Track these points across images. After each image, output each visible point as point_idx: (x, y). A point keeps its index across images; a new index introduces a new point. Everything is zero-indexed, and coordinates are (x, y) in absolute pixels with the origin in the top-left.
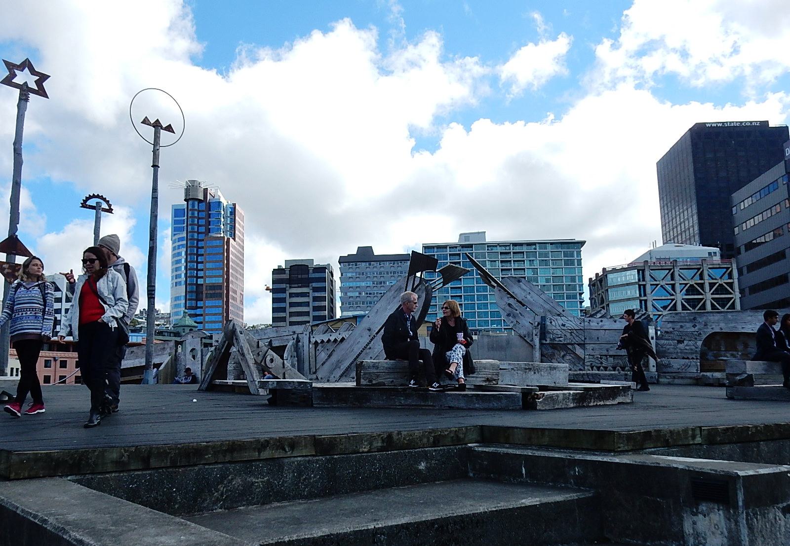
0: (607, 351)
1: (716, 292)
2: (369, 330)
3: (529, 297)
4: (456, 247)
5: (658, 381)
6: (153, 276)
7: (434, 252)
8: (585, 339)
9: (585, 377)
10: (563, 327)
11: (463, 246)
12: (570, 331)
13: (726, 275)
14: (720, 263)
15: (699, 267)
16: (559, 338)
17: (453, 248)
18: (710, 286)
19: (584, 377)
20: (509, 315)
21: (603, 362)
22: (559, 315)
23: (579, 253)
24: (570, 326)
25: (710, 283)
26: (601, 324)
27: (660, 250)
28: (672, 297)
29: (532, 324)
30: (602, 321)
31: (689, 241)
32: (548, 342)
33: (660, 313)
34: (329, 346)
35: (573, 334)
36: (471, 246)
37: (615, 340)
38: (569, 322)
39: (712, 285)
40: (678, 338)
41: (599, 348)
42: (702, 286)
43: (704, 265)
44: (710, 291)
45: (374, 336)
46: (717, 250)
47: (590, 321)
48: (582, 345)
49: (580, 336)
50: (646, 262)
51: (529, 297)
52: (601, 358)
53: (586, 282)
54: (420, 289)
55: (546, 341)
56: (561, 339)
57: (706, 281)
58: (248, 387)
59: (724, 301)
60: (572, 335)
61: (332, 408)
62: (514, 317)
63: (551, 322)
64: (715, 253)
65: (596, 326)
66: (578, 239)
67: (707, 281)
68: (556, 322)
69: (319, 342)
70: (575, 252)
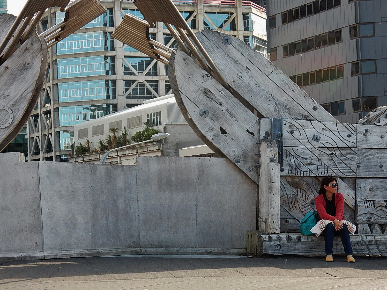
3: (246, 77)
6: (111, 44)
8: (359, 167)
12: (328, 152)
13: (228, 24)
15: (191, 9)
16: (309, 164)
19: (371, 247)
20: (204, 114)
22: (306, 118)
24: (329, 140)
29: (252, 134)
35: (334, 158)
38: (327, 133)
41: (383, 187)
43: (199, 7)
47: (367, 131)
49: (348, 162)
51: (246, 77)
54: (27, 49)
60: (331, 159)
62: (216, 118)
63: (292, 132)
68: (302, 131)
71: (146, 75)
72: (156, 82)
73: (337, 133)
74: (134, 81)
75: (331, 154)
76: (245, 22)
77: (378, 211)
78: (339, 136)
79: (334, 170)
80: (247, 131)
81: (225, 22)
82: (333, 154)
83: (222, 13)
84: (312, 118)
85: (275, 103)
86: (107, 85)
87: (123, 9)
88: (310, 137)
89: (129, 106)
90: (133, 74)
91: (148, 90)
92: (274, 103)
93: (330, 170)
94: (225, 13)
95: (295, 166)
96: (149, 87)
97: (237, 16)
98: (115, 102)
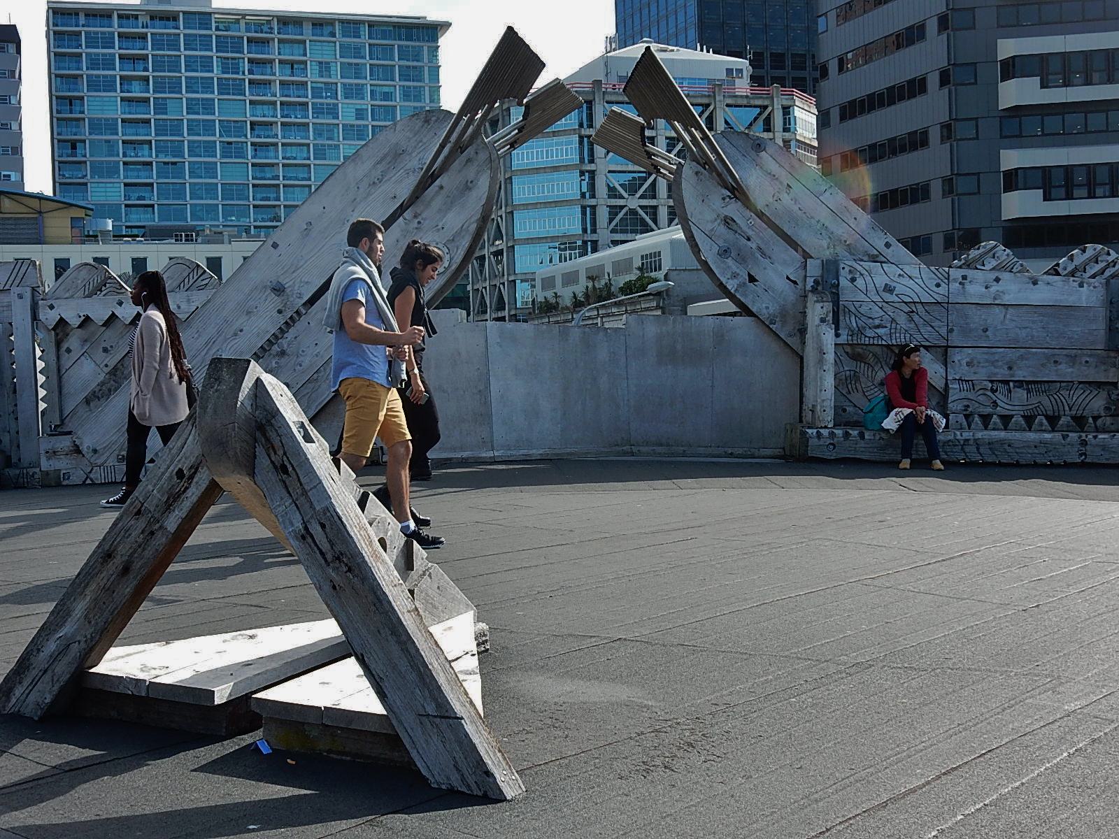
0: (1010, 368)
2: (279, 290)
3: (786, 198)
4: (136, 17)
7: (77, 25)
9: (971, 449)
11: (154, 16)
13: (760, 122)
14: (749, 94)
15: (705, 101)
16: (878, 327)
17: (128, 17)
26: (995, 288)
27: (625, 56)
31: (675, 40)
33: (621, 202)
34: (110, 336)
35: (916, 318)
36: (170, 18)
37: (1033, 337)
38: (906, 281)
41: (987, 361)
45: (298, 312)
46: (742, 63)
47: (964, 277)
48: (944, 353)
50: (597, 83)
52: (993, 391)
56: (881, 331)
58: (394, 741)
62: (742, 259)
63: (853, 280)
64: (740, 71)
65: (982, 296)
66: (433, 16)
69: (75, 322)
70: (425, 49)
72: (655, 208)
74: (622, 207)
76: (785, 119)
78: (923, 286)
80: (788, 278)
82: (913, 312)
83: (750, 106)
86: (584, 213)
89: (616, 243)
91: (643, 220)
97: (773, 110)
98: (594, 237)
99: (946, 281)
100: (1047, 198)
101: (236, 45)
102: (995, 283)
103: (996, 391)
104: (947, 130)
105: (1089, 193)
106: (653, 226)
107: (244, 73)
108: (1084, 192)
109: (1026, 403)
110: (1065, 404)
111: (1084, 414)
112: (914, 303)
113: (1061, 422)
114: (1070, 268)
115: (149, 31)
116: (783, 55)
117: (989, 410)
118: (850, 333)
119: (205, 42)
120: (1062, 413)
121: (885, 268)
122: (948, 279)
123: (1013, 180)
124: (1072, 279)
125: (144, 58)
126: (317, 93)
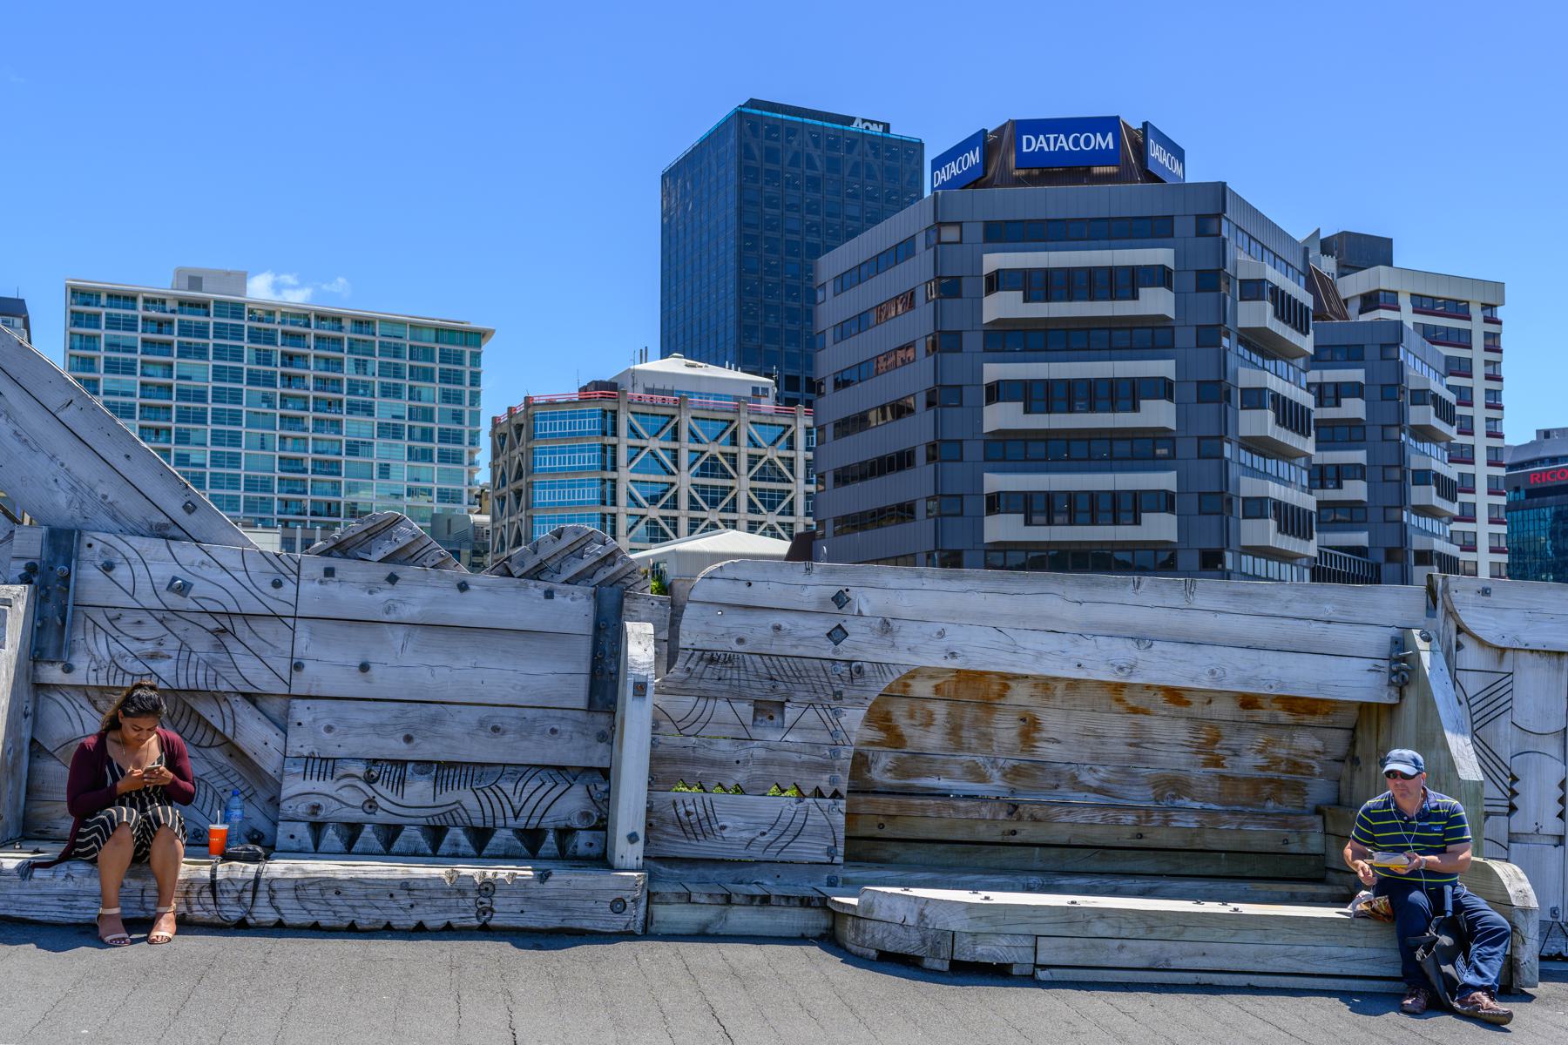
1: (726, 491)
4: (163, 302)
5: (648, 919)
10: (173, 600)
12: (213, 625)
13: (784, 439)
15: (729, 416)
18: (749, 462)
21: (381, 802)
23: (476, 358)
25: (750, 456)
28: (671, 479)
30: (392, 579)
32: (78, 678)
33: (641, 511)
36: (200, 306)
39: (753, 459)
40: (759, 690)
42: (733, 459)
44: (750, 469)
52: (370, 780)
53: (485, 427)
55: (68, 669)
57: (742, 449)
59: (774, 496)
61: (28, 635)
63: (108, 567)
64: (765, 390)
66: (476, 324)
67: (744, 450)
68: (139, 569)
71: (661, 508)
73: (241, 576)
75: (221, 631)
76: (808, 439)
77: (341, 788)
78: (248, 584)
79: (224, 675)
81: (779, 437)
82: (225, 630)
83: (774, 425)
84: (177, 532)
85: (73, 487)
87: (632, 413)
88: (161, 583)
90: (702, 509)
91: (662, 530)
92: (70, 486)
93: (214, 673)
94: (779, 425)
95: (108, 659)
96: (664, 526)
97: (796, 429)
99: (294, 577)
100: (1028, 522)
101: (270, 337)
102: (388, 586)
103: (375, 781)
104: (934, 453)
105: (1070, 520)
106: (671, 534)
107: (276, 366)
108: (1043, 519)
109: (433, 804)
110: (507, 807)
111: (543, 825)
112: (229, 614)
113: (493, 841)
114: (531, 563)
115: (176, 317)
116: (797, 378)
117: (358, 815)
118: (94, 665)
119: (237, 333)
120: (500, 822)
121: (175, 550)
122: (298, 575)
123: (995, 503)
124: (532, 583)
125: (169, 344)
126: (353, 390)
